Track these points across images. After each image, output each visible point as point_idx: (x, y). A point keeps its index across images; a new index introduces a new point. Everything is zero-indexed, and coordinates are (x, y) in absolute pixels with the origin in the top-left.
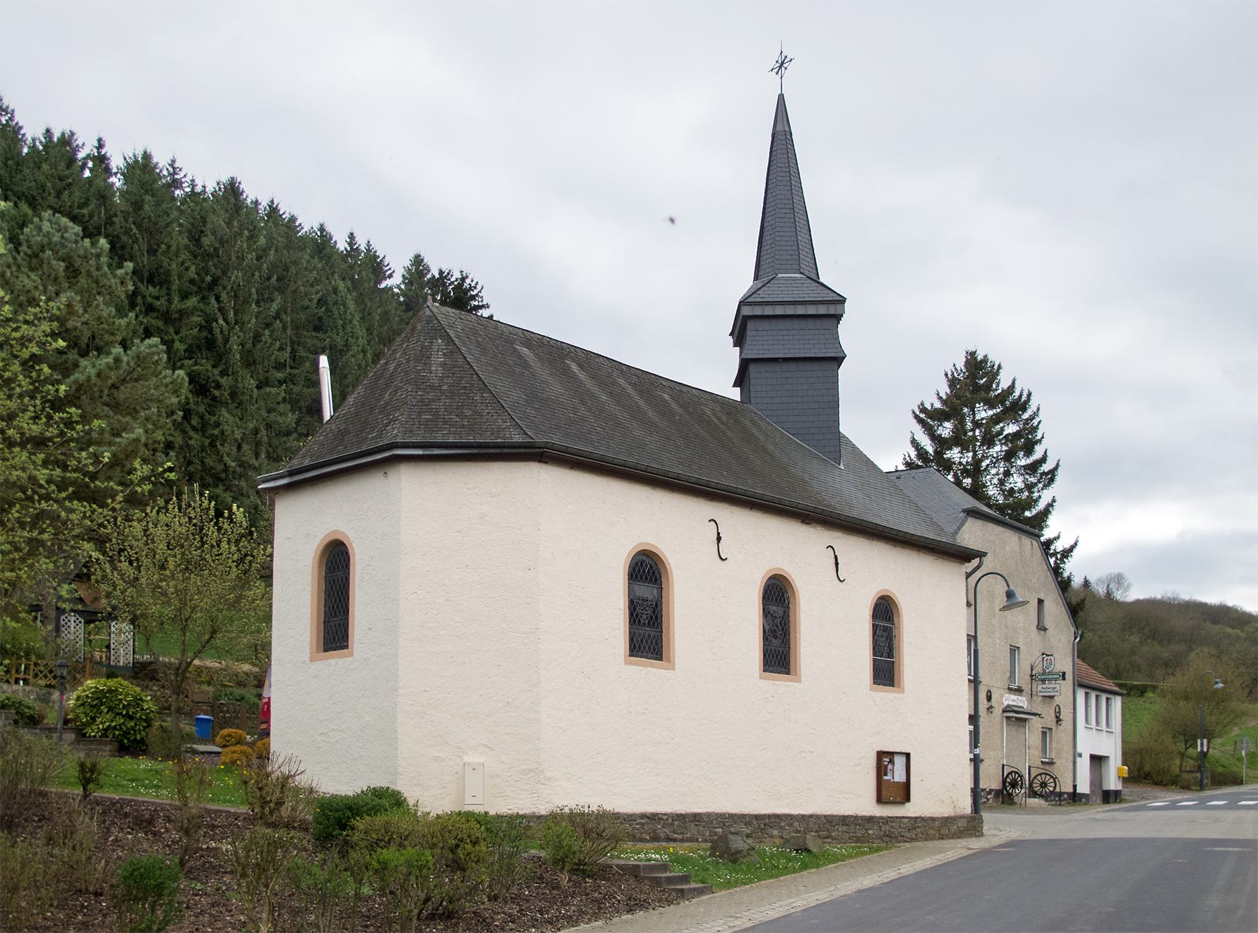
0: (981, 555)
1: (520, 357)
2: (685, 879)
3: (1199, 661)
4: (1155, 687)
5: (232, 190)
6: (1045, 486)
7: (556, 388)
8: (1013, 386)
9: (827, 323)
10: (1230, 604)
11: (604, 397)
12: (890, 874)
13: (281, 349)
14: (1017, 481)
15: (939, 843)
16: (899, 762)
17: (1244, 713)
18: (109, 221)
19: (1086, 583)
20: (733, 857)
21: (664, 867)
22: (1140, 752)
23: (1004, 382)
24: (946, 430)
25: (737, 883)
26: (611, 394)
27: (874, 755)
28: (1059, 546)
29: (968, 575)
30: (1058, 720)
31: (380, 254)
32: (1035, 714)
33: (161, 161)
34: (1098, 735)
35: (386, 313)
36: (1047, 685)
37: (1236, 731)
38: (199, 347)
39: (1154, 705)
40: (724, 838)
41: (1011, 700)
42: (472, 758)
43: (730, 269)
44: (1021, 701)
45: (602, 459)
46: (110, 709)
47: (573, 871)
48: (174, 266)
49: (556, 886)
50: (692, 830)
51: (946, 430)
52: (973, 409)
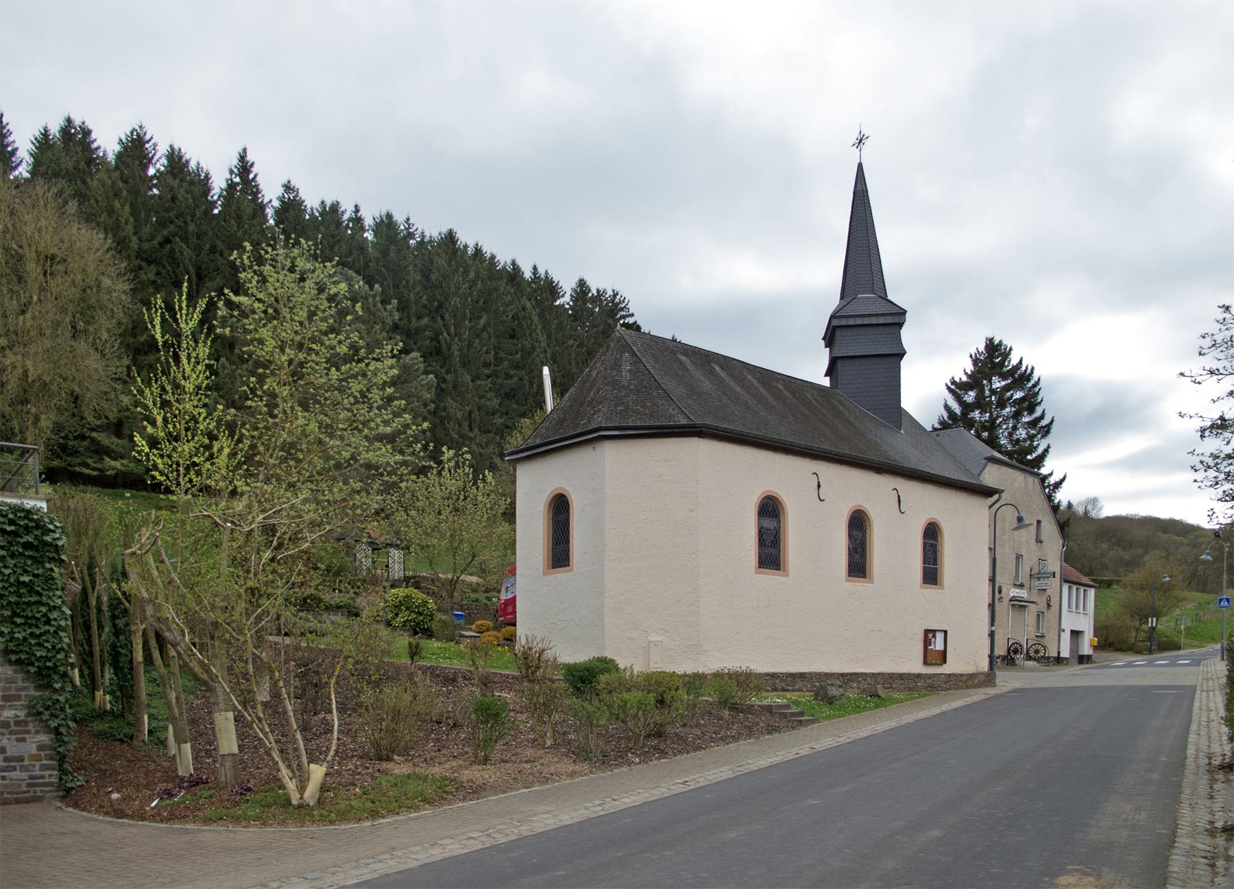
1: (681, 363)
2: (801, 714)
3: (1152, 561)
4: (1118, 581)
5: (450, 237)
6: (1043, 437)
7: (706, 385)
9: (893, 329)
10: (1177, 518)
11: (738, 389)
12: (935, 711)
13: (487, 352)
14: (1022, 433)
15: (966, 691)
16: (940, 636)
17: (1184, 599)
18: (366, 266)
19: (1070, 505)
20: (831, 701)
21: (788, 706)
22: (1106, 627)
23: (1014, 360)
24: (970, 396)
25: (835, 716)
26: (743, 387)
28: (1052, 480)
30: (1049, 606)
31: (556, 280)
33: (399, 218)
34: (1078, 616)
35: (560, 323)
36: (1042, 581)
37: (1178, 611)
38: (431, 354)
39: (1118, 594)
40: (823, 688)
41: (1015, 592)
42: (654, 638)
44: (1023, 593)
45: (741, 434)
46: (407, 608)
47: (730, 709)
48: (412, 296)
49: (721, 718)
50: (799, 684)
51: (970, 396)
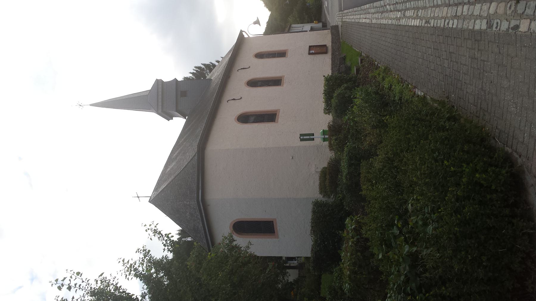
8: (191, 73)
43: (152, 119)
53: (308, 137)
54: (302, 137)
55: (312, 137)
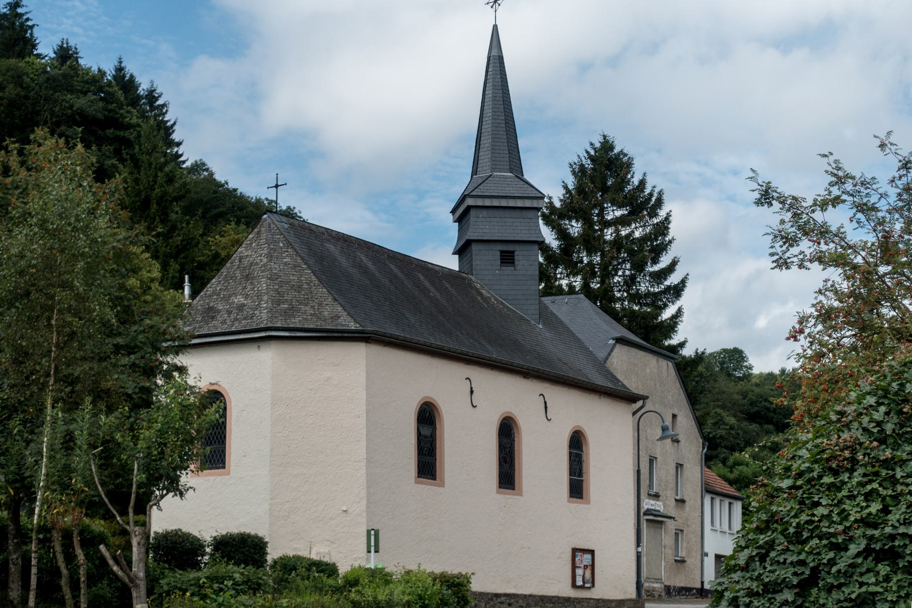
0: (645, 398)
27: (591, 548)
29: (634, 414)
32: (670, 518)
52: (602, 210)
53: (373, 543)
54: (373, 532)
55: (373, 549)
